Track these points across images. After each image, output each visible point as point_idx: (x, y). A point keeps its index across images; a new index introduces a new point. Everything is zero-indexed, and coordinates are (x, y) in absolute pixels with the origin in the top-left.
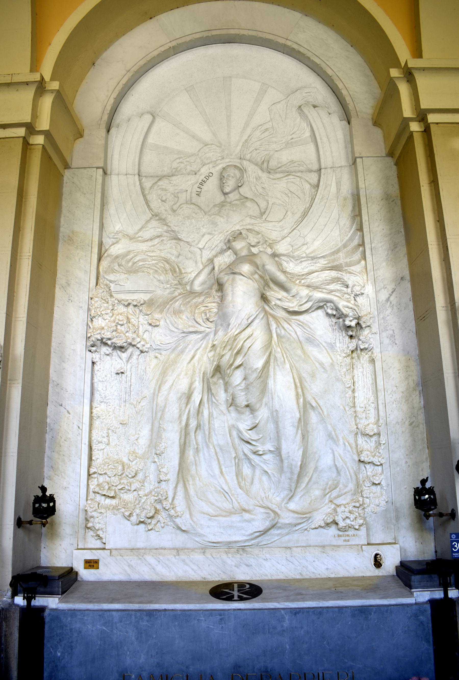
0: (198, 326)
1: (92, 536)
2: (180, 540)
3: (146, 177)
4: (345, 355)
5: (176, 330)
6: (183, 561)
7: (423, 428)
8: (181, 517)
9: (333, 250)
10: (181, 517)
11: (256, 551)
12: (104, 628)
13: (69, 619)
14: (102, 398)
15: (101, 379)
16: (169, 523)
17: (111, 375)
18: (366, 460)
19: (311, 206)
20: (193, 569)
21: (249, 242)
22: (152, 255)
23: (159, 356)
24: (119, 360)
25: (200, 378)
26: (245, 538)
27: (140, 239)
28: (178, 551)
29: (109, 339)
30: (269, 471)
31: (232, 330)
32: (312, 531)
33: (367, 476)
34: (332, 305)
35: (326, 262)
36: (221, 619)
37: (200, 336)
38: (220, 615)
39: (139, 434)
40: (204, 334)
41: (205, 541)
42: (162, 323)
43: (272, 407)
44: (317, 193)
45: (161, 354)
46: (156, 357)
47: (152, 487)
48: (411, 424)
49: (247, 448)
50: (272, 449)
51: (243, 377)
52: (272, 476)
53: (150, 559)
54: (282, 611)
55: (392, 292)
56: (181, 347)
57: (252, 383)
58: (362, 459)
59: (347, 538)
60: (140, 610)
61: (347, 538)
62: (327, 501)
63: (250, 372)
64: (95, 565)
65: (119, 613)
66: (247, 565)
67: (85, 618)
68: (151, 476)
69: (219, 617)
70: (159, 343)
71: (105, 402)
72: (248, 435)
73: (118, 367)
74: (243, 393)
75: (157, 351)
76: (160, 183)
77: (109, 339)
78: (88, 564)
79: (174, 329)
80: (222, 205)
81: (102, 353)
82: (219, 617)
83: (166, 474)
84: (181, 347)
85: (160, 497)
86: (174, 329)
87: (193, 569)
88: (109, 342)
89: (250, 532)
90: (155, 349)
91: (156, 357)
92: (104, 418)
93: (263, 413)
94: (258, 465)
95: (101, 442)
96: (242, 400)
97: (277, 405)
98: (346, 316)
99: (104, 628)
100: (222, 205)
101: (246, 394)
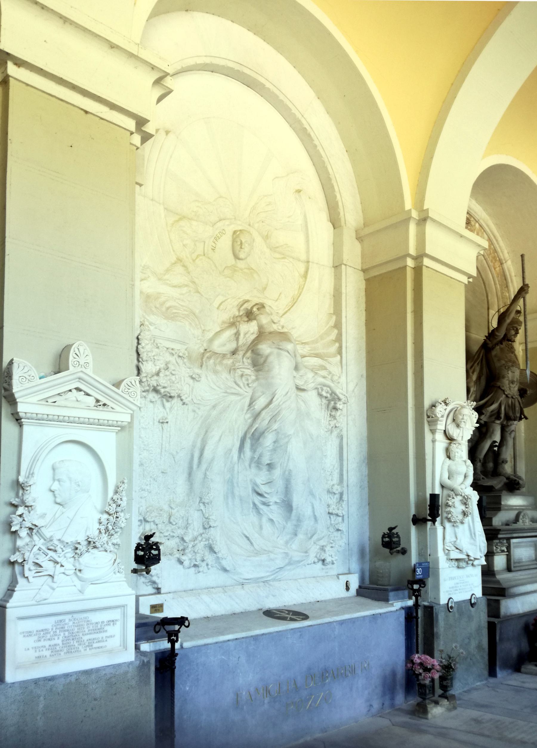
0: (237, 388)
1: (143, 583)
2: (221, 578)
3: (299, 260)
4: (326, 430)
5: (218, 389)
6: (230, 596)
7: (366, 490)
8: (225, 559)
9: (313, 339)
10: (225, 559)
11: (276, 584)
12: (223, 657)
13: (196, 655)
14: (145, 445)
15: (144, 426)
16: (214, 565)
17: (154, 424)
18: (334, 512)
19: (300, 295)
20: (237, 603)
21: (273, 318)
22: (182, 304)
23: (197, 411)
24: (161, 409)
25: (238, 436)
26: (268, 574)
27: (168, 282)
28: (224, 588)
29: (164, 387)
30: (274, 519)
31: (278, 399)
32: (307, 566)
33: (331, 524)
34: (329, 389)
35: (309, 349)
36: (301, 635)
37: (239, 398)
38: (300, 632)
39: (176, 483)
40: (242, 397)
41: (241, 578)
42: (203, 379)
43: (286, 467)
44: (305, 284)
45: (199, 409)
46: (194, 411)
47: (196, 534)
48: (360, 487)
49: (257, 500)
50: (278, 501)
51: (274, 440)
52: (276, 523)
53: (205, 598)
54: (335, 623)
55: (356, 385)
56: (222, 405)
57: (281, 446)
58: (331, 511)
59: (327, 571)
60: (246, 638)
61: (327, 571)
62: (312, 543)
63: (283, 436)
64: (160, 609)
65: (234, 642)
66: (274, 596)
67: (209, 651)
68: (195, 523)
69: (299, 634)
70: (200, 398)
71: (147, 450)
72: (263, 489)
73: (160, 416)
74: (268, 454)
75: (196, 405)
76: (182, 223)
77: (164, 387)
78: (154, 609)
79: (215, 387)
80: (234, 269)
81: (148, 399)
82: (299, 634)
83: (215, 521)
84: (222, 405)
85: (211, 542)
86: (215, 387)
87: (237, 603)
88: (162, 390)
89: (273, 568)
90: (195, 403)
91: (194, 411)
92: (147, 465)
93: (277, 472)
94: (266, 514)
95: (144, 490)
96: (266, 460)
97: (291, 466)
98: (339, 400)
99: (223, 657)
100: (234, 269)
101: (271, 455)
